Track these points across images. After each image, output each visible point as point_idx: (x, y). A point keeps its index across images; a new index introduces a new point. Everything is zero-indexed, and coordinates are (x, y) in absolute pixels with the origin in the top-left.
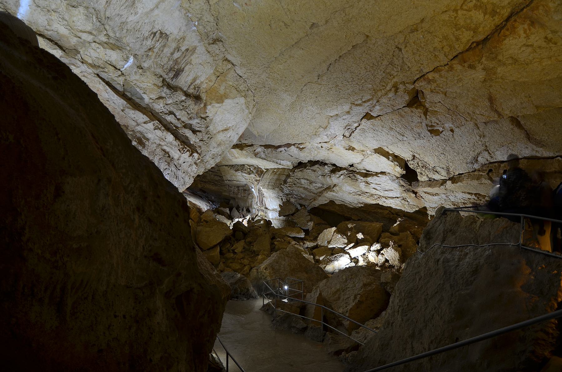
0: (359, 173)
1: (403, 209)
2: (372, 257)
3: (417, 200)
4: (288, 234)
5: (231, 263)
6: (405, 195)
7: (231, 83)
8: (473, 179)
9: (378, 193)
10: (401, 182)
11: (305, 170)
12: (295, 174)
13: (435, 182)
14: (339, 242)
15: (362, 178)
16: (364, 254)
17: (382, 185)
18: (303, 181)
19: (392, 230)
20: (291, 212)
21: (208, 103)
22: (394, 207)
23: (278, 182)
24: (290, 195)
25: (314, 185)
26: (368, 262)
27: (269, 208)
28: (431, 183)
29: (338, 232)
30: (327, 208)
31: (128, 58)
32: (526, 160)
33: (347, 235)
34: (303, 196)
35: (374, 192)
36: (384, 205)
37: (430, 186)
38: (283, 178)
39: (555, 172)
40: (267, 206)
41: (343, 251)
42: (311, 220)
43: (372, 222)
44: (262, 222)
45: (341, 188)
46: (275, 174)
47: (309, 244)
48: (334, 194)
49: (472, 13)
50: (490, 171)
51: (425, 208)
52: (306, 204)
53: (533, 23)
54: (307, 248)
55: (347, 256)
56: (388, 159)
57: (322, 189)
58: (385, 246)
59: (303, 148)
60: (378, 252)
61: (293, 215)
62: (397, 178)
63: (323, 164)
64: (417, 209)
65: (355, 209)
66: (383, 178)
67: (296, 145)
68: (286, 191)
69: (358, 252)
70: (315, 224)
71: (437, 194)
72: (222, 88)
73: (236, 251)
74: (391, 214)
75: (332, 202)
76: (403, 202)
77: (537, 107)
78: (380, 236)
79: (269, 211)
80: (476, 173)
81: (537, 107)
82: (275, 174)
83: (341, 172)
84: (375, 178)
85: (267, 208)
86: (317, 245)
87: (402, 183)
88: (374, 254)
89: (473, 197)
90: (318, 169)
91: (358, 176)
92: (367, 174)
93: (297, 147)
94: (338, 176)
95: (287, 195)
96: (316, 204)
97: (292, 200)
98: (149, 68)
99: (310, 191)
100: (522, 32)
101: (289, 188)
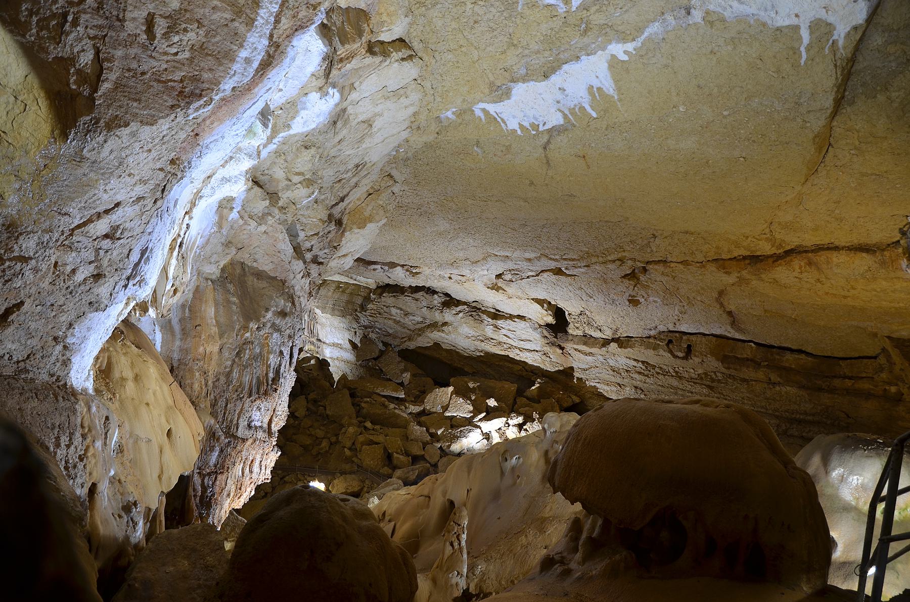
0: (484, 312)
1: (542, 366)
2: (512, 433)
3: (563, 357)
4: (378, 391)
5: (294, 434)
6: (547, 349)
7: (381, 203)
8: (647, 347)
9: (509, 341)
10: (545, 332)
11: (402, 297)
12: (383, 299)
13: (593, 340)
14: (461, 409)
15: (490, 320)
16: (500, 429)
17: (518, 333)
18: (394, 311)
19: (528, 393)
20: (374, 355)
21: (348, 228)
22: (530, 362)
23: (350, 307)
24: (371, 327)
25: (411, 318)
26: (507, 440)
27: (324, 340)
28: (587, 339)
29: (457, 392)
30: (427, 352)
31: (313, 193)
32: (715, 339)
33: (471, 400)
34: (391, 331)
35: (505, 339)
36: (518, 358)
37: (585, 344)
38: (359, 301)
39: (748, 359)
40: (320, 337)
41: (469, 423)
42: (405, 370)
43: (505, 383)
44: (313, 362)
45: (456, 328)
46: (343, 292)
47: (415, 409)
48: (443, 335)
49: (760, 243)
50: (670, 342)
51: (572, 368)
52: (395, 342)
53: (810, 264)
54: (410, 413)
55: (479, 430)
56: (543, 307)
57: (423, 325)
58: (528, 419)
59: (417, 273)
60: (520, 427)
61: (375, 359)
62: (540, 326)
63: (431, 291)
64: (561, 368)
65: (470, 358)
66: (521, 324)
67: (406, 267)
68: (364, 321)
69: (492, 426)
70: (413, 375)
71: (591, 354)
72: (370, 208)
73: (296, 414)
74: (525, 374)
75: (437, 345)
76: (544, 357)
77: (766, 311)
78: (515, 402)
79: (324, 346)
80: (651, 340)
81: (766, 311)
82: (343, 292)
83: (460, 308)
84: (509, 322)
85: (319, 340)
86: (424, 409)
87: (546, 333)
88: (515, 429)
89: (640, 365)
90: (422, 298)
91: (485, 317)
92: (497, 315)
93: (407, 270)
94: (454, 312)
95: (366, 327)
96: (412, 345)
97: (373, 336)
98: (323, 200)
99: (404, 326)
100: (797, 267)
101: (370, 318)
